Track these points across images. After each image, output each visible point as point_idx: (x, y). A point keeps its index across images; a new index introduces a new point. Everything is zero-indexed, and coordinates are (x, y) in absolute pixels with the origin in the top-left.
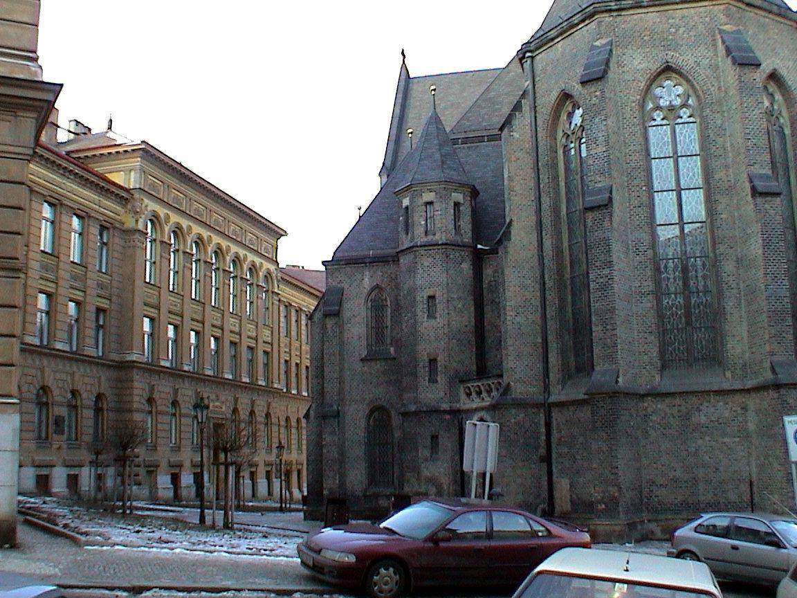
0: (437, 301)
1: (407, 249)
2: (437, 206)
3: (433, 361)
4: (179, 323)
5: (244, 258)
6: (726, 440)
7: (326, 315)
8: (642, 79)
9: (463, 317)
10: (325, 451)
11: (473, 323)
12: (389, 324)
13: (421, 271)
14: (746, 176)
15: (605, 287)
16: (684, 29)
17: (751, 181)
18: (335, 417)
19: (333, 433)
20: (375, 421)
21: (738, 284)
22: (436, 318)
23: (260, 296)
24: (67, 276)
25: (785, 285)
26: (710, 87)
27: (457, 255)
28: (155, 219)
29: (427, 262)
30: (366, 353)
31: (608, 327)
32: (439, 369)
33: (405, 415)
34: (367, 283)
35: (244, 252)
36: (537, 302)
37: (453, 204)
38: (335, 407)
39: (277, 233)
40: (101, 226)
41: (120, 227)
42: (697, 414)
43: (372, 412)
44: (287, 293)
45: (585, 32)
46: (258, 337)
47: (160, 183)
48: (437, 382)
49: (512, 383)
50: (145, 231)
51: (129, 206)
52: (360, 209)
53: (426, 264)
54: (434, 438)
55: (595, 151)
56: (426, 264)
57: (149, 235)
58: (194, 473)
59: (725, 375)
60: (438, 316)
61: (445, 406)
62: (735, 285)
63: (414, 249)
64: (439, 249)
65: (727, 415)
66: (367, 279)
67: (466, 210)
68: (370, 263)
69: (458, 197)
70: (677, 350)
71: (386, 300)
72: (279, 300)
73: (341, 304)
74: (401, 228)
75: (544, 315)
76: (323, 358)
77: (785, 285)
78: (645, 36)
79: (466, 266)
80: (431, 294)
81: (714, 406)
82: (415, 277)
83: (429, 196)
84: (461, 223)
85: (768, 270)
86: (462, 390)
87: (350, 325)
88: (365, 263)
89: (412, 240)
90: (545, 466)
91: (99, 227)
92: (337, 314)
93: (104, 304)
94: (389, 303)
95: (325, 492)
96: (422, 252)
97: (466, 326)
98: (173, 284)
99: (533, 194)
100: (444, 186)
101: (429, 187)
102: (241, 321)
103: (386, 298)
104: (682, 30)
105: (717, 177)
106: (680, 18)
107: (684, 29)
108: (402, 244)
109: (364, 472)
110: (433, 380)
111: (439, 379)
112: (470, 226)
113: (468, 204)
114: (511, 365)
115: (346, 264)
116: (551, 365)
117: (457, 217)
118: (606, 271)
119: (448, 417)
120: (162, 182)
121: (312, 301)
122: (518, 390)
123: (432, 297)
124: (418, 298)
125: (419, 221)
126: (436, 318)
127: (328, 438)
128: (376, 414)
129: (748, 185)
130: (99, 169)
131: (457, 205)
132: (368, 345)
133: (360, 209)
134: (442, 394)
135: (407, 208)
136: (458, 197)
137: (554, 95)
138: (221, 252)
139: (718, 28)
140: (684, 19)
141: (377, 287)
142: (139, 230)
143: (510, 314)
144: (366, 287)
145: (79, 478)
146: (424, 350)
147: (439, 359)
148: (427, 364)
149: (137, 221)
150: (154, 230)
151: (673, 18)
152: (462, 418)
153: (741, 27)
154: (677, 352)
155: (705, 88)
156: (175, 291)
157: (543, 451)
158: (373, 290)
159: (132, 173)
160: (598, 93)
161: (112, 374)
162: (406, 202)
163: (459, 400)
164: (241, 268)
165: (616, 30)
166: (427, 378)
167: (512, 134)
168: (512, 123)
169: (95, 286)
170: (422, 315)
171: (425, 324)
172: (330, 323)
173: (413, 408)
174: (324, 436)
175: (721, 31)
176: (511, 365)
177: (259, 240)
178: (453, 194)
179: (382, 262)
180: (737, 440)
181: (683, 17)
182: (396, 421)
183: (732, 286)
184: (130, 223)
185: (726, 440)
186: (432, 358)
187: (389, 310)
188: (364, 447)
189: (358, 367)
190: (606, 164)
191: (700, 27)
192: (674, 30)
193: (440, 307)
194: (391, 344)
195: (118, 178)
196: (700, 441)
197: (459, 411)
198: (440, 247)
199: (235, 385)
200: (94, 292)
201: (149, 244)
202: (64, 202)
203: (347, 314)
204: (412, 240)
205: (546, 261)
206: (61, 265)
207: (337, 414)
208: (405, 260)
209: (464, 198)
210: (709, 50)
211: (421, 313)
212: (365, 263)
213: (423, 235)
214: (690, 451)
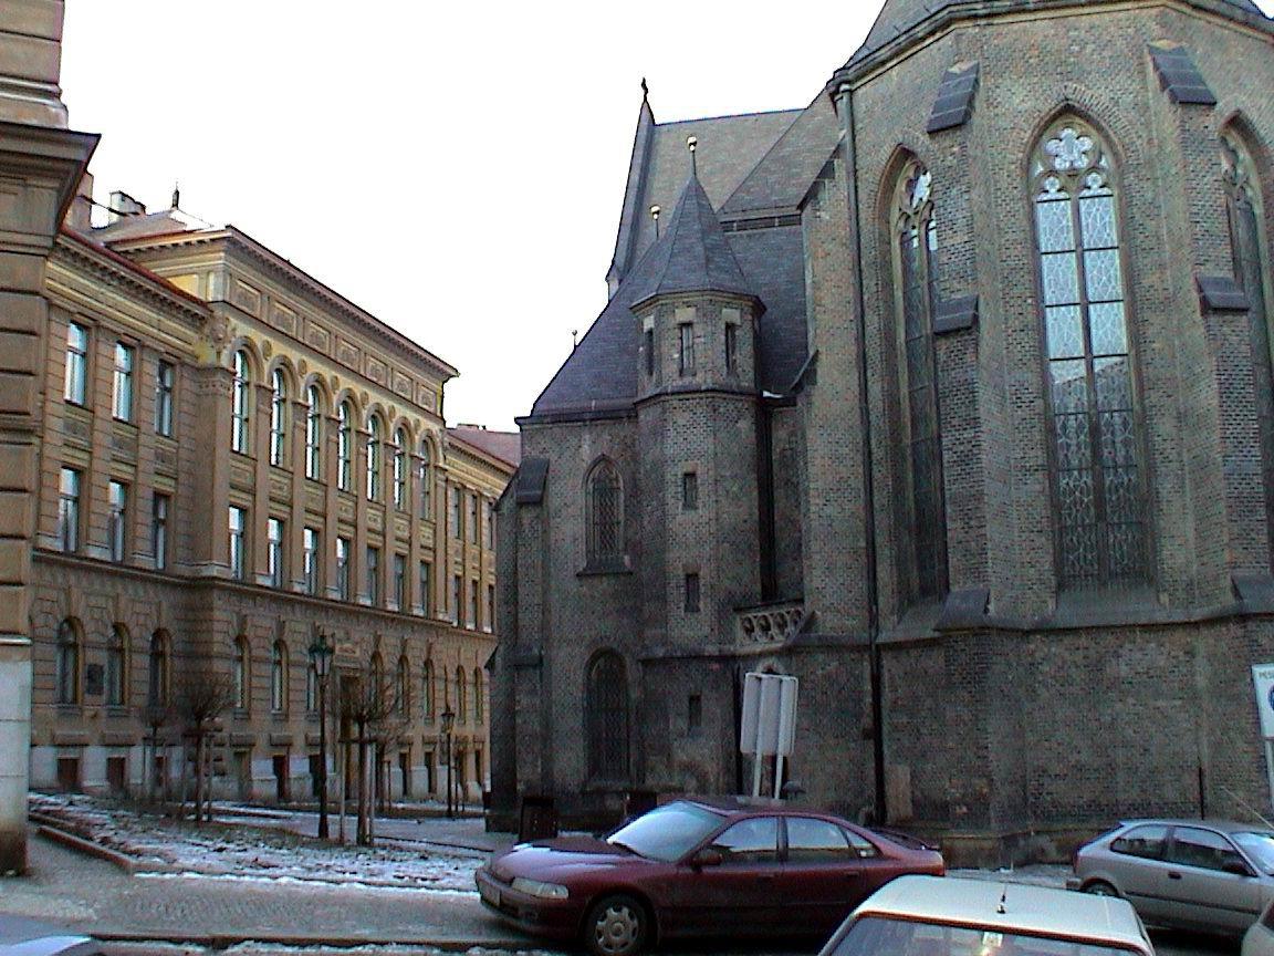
0: (699, 481)
1: (650, 398)
2: (698, 329)
3: (692, 578)
4: (286, 516)
5: (390, 413)
6: (1160, 703)
7: (521, 504)
8: (1026, 127)
9: (741, 506)
10: (519, 721)
11: (756, 517)
12: (622, 518)
13: (672, 433)
14: (1192, 281)
15: (967, 459)
16: (1093, 46)
17: (1200, 290)
18: (535, 667)
19: (533, 692)
20: (599, 672)
21: (1179, 454)
22: (696, 508)
23: (415, 472)
24: (107, 441)
25: (1255, 456)
26: (1135, 139)
27: (731, 407)
28: (247, 351)
29: (682, 419)
30: (585, 564)
31: (972, 523)
32: (702, 590)
33: (648, 663)
34: (587, 452)
35: (391, 403)
36: (858, 483)
37: (723, 327)
38: (536, 651)
39: (442, 372)
40: (161, 361)
41: (192, 363)
42: (1114, 662)
43: (594, 658)
44: (459, 469)
45: (935, 51)
46: (413, 539)
47: (256, 293)
48: (698, 610)
49: (819, 613)
50: (231, 369)
51: (207, 330)
52: (575, 334)
53: (681, 422)
54: (695, 700)
55: (952, 242)
56: (681, 422)
57: (239, 375)
58: (310, 757)
59: (1158, 600)
60: (701, 505)
61: (711, 649)
62: (1176, 455)
63: (663, 398)
64: (701, 398)
65: (1162, 663)
66: (586, 447)
67: (744, 336)
68: (592, 420)
69: (732, 315)
70: (1082, 559)
71: (617, 479)
72: (447, 480)
73: (544, 486)
74: (641, 365)
75: (870, 504)
76: (516, 573)
77: (1255, 456)
78: (1030, 58)
79: (745, 426)
80: (690, 470)
81: (1141, 649)
82: (663, 443)
83: (685, 314)
84: (737, 356)
85: (1228, 432)
86: (738, 623)
87: (559, 520)
88: (584, 421)
89: (659, 383)
90: (870, 744)
91: (158, 363)
92: (539, 502)
93: (166, 485)
94: (621, 484)
95: (520, 787)
96: (675, 403)
97: (745, 521)
98: (277, 455)
99: (852, 310)
100: (710, 297)
101: (686, 300)
102: (384, 512)
103: (617, 477)
104: (1090, 48)
105: (1146, 283)
106: (1087, 28)
107: (1093, 46)
108: (643, 390)
109: (582, 755)
110: (692, 608)
111: (701, 605)
112: (751, 361)
113: (748, 325)
114: (817, 583)
115: (553, 423)
116: (880, 584)
117: (730, 347)
118: (969, 434)
119: (716, 666)
120: (259, 291)
121: (498, 481)
122: (829, 624)
123: (690, 476)
124: (668, 476)
125: (670, 353)
126: (696, 508)
127: (524, 701)
128: (601, 662)
129: (1195, 296)
130: (159, 270)
131: (730, 327)
132: (588, 552)
133: (575, 334)
134: (707, 630)
135: (650, 332)
136: (732, 315)
137: (886, 152)
138: (354, 403)
139: (1148, 46)
140: (1093, 31)
141: (603, 459)
142: (223, 368)
143: (815, 503)
144: (586, 458)
145: (127, 764)
146: (678, 560)
147: (701, 573)
148: (683, 582)
149: (219, 353)
150: (246, 368)
151: (1076, 29)
152: (739, 668)
153: (1184, 44)
154: (1082, 563)
155: (1127, 140)
156: (281, 465)
157: (867, 722)
158: (596, 463)
159: (212, 277)
160: (955, 149)
161: (179, 597)
162: (649, 323)
163: (734, 640)
164: (385, 429)
165: (985, 47)
166: (682, 605)
167: (818, 213)
168: (819, 197)
169: (152, 458)
170: (674, 504)
171: (680, 518)
172: (527, 516)
173: (660, 652)
174: (517, 698)
175: (1152, 50)
176: (817, 583)
177: (414, 384)
178: (724, 310)
179: (611, 418)
180: (1178, 703)
181: (1091, 28)
182: (633, 672)
183: (1171, 457)
184: (207, 356)
185: (1160, 703)
186: (690, 572)
187: (622, 495)
188: (581, 715)
189: (573, 586)
190: (968, 262)
191: (1120, 43)
192: (1077, 48)
193: (703, 491)
194: (625, 550)
195: (188, 285)
196: (1119, 706)
197: (734, 657)
198: (703, 395)
199: (376, 615)
200: (151, 468)
201: (238, 391)
202: (103, 323)
203: (554, 502)
204: (659, 383)
205: (873, 418)
206: (98, 423)
207: (539, 662)
208: (647, 416)
209: (741, 317)
210: (1134, 81)
211: (673, 501)
212: (584, 421)
213: (676, 376)
214: (1102, 720)
